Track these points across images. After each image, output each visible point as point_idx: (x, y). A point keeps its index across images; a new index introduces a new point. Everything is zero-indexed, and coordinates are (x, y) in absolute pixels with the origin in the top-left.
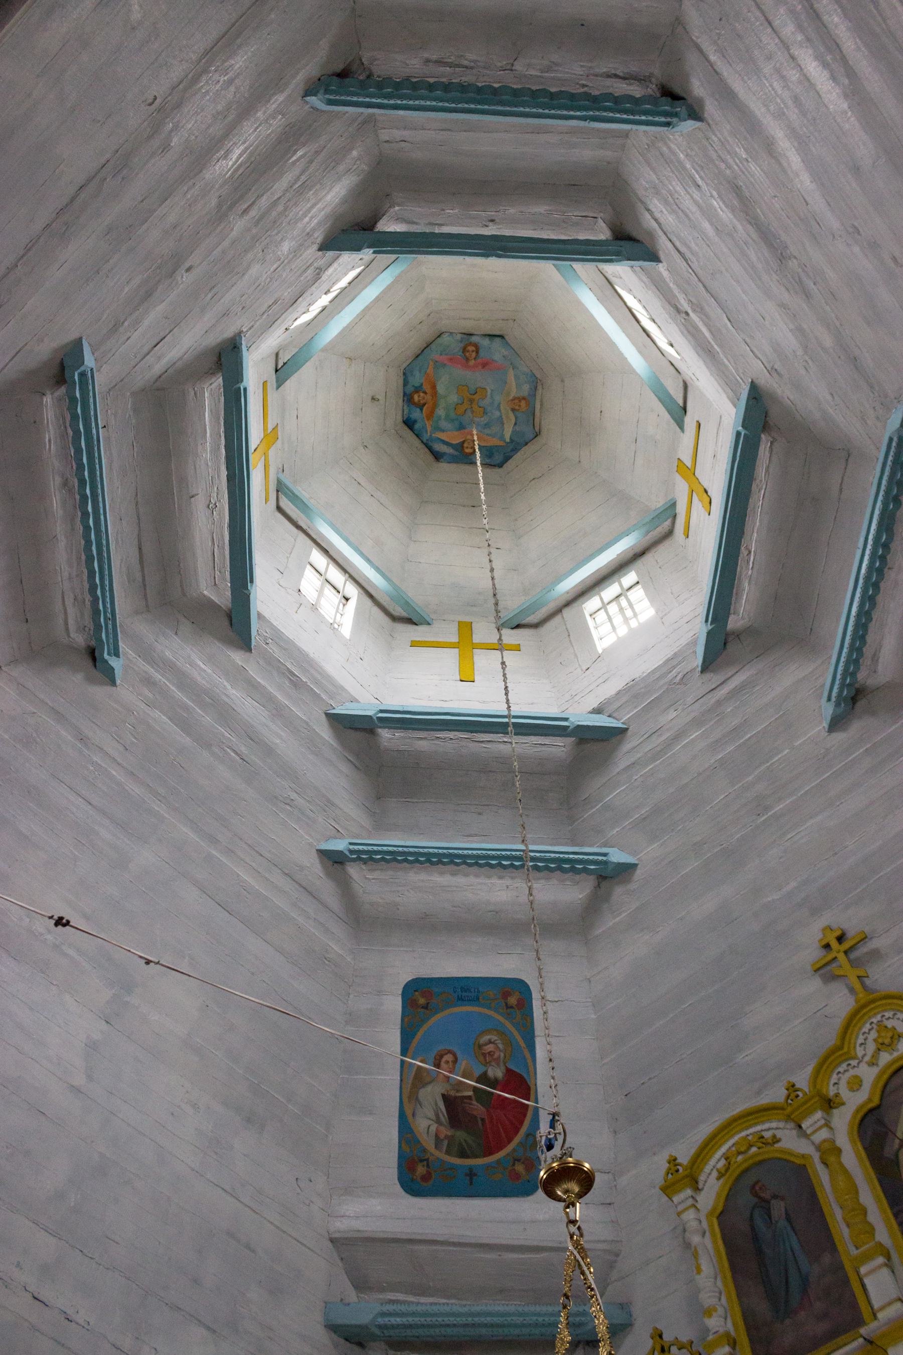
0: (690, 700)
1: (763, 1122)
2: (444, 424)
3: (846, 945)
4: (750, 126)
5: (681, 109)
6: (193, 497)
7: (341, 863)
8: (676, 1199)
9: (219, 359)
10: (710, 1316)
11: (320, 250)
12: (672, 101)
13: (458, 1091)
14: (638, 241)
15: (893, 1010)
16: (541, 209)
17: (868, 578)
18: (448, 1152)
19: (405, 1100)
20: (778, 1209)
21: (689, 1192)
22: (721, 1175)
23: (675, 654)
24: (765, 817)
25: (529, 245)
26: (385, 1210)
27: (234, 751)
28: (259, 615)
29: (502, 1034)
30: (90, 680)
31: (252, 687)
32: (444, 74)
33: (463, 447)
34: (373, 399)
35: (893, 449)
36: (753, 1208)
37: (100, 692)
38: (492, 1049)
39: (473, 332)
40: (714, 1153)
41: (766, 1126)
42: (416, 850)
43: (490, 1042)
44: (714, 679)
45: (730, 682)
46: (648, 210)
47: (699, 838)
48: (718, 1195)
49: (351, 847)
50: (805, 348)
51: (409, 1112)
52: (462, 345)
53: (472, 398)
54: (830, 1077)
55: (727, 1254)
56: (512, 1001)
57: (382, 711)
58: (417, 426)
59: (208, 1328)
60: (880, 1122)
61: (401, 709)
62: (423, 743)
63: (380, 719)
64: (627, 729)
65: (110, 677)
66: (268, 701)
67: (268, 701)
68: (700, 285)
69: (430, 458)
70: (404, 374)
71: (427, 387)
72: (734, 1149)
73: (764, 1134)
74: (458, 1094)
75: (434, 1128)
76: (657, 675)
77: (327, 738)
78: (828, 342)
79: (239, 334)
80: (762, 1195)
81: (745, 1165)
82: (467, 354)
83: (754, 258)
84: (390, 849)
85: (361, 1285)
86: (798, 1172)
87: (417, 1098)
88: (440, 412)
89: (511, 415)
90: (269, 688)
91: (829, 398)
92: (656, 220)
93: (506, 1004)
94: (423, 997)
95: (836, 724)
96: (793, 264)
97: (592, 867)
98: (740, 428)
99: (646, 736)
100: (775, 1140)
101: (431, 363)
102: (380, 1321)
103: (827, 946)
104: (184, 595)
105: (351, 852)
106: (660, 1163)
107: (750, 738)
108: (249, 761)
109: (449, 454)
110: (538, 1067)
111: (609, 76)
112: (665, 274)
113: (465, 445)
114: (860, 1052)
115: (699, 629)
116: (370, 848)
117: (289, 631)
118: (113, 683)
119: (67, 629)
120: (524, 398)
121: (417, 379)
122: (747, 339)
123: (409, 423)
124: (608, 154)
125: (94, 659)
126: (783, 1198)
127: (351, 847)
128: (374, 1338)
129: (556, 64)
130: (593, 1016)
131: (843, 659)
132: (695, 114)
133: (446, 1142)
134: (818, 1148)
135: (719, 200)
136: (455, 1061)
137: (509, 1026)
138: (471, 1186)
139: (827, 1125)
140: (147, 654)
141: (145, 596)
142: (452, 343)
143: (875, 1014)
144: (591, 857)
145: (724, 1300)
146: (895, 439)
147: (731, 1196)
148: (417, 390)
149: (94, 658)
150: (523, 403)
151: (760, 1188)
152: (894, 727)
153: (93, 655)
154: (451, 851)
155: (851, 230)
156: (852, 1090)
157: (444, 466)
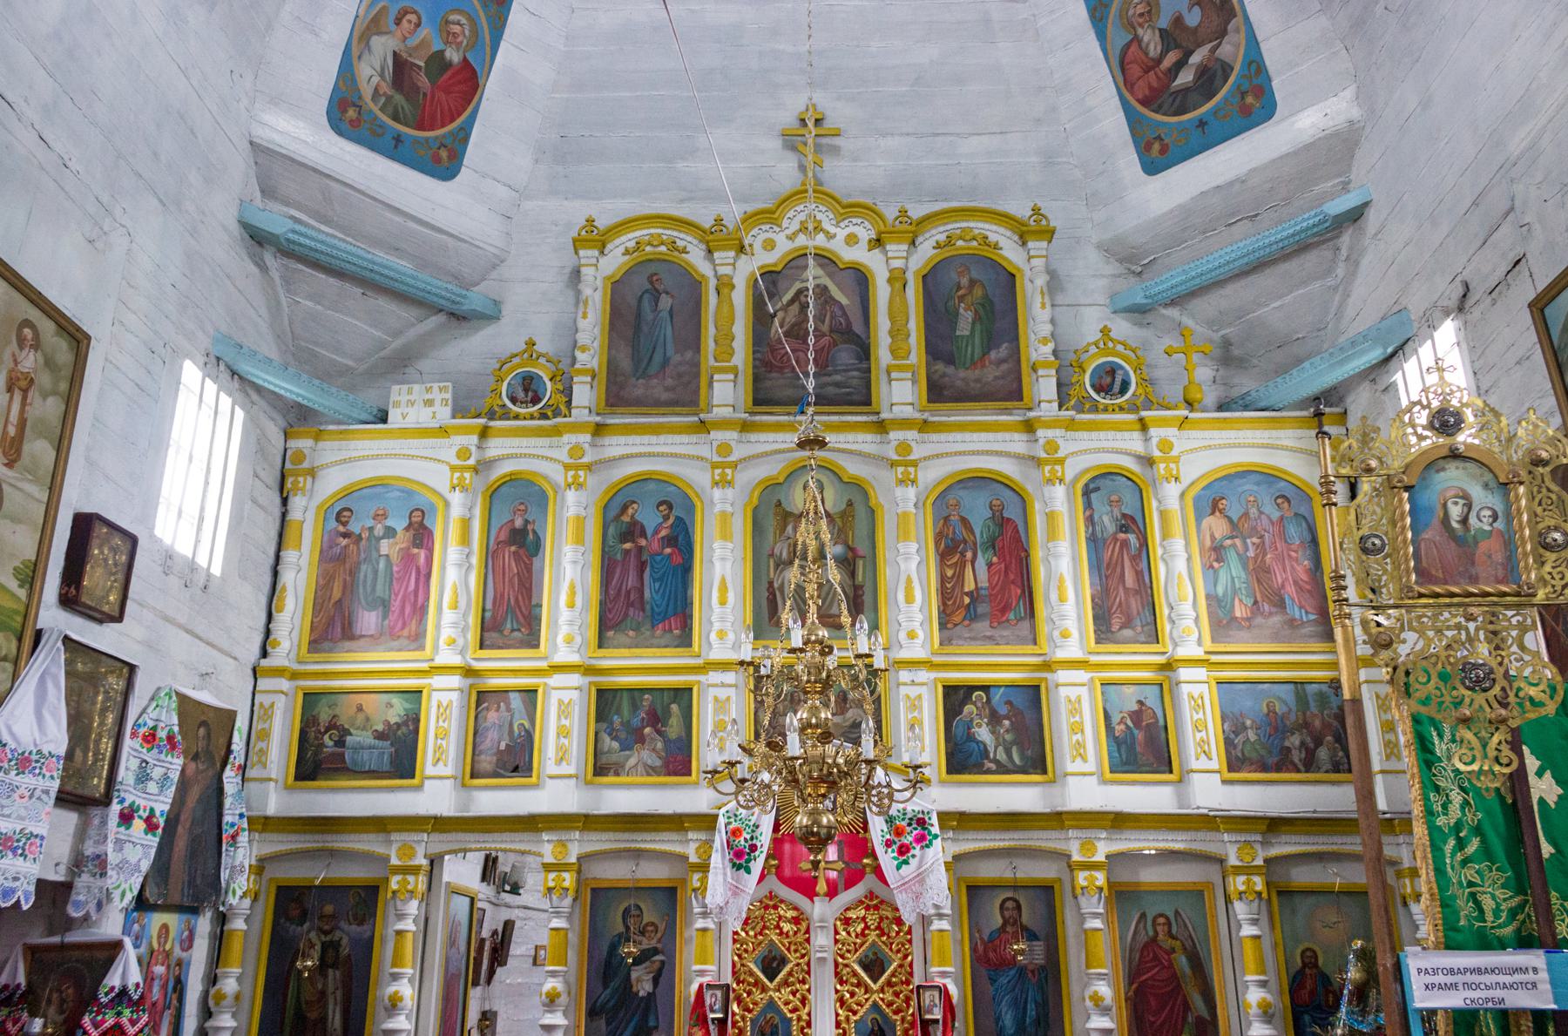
19: (355, 43)
20: (665, 302)
21: (596, 253)
22: (627, 252)
26: (305, 134)
29: (473, 21)
48: (620, 268)
51: (355, 52)
59: (161, 201)
75: (376, 79)
85: (268, 192)
86: (694, 286)
102: (291, 236)
106: (576, 212)
128: (270, 243)
133: (383, 100)
136: (418, 25)
137: (482, 14)
138: (395, 150)
156: (765, 248)
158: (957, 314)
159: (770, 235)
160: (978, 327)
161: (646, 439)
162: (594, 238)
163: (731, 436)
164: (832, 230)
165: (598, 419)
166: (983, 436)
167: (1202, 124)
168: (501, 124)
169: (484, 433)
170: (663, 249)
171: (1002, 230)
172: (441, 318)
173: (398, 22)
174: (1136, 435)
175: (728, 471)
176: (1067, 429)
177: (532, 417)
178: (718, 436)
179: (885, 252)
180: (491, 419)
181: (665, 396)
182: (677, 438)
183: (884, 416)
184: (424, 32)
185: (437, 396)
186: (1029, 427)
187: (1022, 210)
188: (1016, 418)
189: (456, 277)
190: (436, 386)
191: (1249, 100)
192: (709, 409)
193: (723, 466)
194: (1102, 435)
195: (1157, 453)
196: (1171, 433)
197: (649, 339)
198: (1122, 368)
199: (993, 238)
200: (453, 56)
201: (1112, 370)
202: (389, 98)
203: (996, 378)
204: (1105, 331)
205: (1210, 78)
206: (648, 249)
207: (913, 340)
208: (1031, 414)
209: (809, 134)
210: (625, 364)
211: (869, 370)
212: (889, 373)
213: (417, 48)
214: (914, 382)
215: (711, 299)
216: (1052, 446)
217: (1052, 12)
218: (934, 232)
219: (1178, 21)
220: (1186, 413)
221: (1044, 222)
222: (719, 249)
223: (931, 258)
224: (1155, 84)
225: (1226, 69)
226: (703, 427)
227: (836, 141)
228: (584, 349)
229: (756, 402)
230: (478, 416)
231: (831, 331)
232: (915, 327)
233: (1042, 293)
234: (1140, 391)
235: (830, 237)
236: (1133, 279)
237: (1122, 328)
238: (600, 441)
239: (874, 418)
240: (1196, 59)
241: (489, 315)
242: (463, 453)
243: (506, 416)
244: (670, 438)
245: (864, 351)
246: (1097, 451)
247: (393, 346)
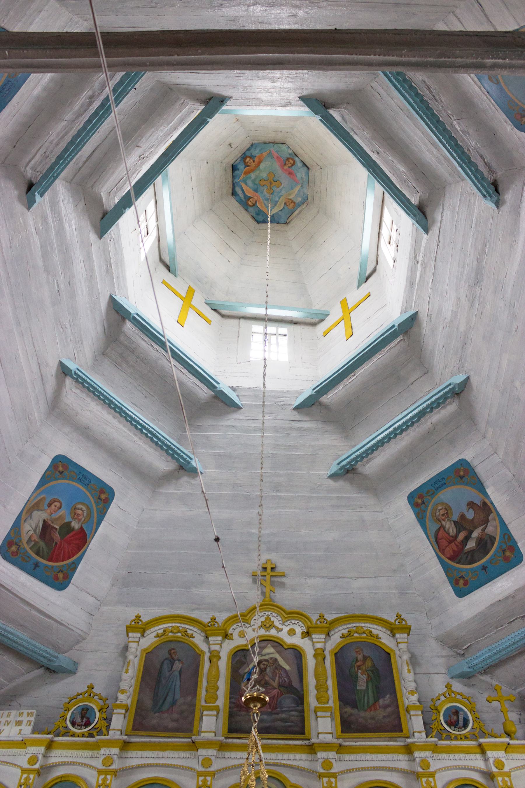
0: (279, 417)
1: (190, 625)
2: (249, 182)
3: (273, 574)
4: (514, 230)
5: (495, 198)
6: (138, 146)
7: (66, 375)
9: (210, 99)
10: (123, 693)
11: (299, 97)
12: (494, 190)
13: (52, 523)
14: (425, 217)
15: (278, 614)
16: (402, 168)
17: (396, 429)
18: (31, 548)
20: (177, 666)
21: (139, 635)
22: (157, 636)
23: (288, 391)
24: (275, 494)
25: (387, 181)
27: (57, 283)
28: (118, 223)
29: (89, 509)
31: (89, 257)
32: (424, 91)
33: (249, 200)
34: (230, 145)
35: (448, 389)
36: (166, 659)
37: (19, 208)
38: (80, 513)
39: (299, 156)
40: (160, 625)
41: (191, 628)
42: (107, 395)
43: (81, 509)
44: (296, 416)
45: (303, 423)
46: (443, 212)
47: (239, 482)
49: (77, 371)
50: (451, 321)
51: (23, 517)
52: (289, 156)
53: (272, 182)
54: (233, 625)
55: (143, 671)
56: (103, 496)
58: (237, 172)
60: (245, 657)
61: (147, 320)
62: (144, 344)
63: (134, 317)
64: (242, 408)
65: (30, 204)
66: (90, 270)
67: (90, 270)
68: (434, 258)
69: (231, 191)
70: (252, 145)
71: (256, 160)
72: (170, 628)
73: (188, 631)
74: (52, 524)
75: (31, 533)
76: (273, 394)
77: (102, 308)
78: (462, 328)
79: (230, 98)
80: (173, 656)
81: (171, 639)
82: (287, 162)
83: (466, 272)
84: (95, 386)
86: (196, 657)
87: (31, 514)
88: (253, 175)
89: (283, 205)
90: (95, 264)
91: (441, 347)
92: (442, 219)
93: (99, 496)
94: (62, 467)
95: (334, 476)
96: (478, 290)
97: (181, 460)
98: (396, 325)
99: (247, 418)
100: (192, 636)
101: (268, 151)
103: (265, 569)
104: (92, 186)
105: (75, 373)
107: (293, 454)
108: (61, 294)
109: (240, 198)
110: (96, 534)
111: (482, 157)
112: (424, 241)
113: (251, 200)
114: (252, 623)
115: (308, 392)
116: (86, 378)
117: (124, 242)
118: (29, 208)
119: (28, 164)
120: (294, 203)
121: (255, 152)
122: (432, 295)
123: (234, 168)
124: (449, 178)
126: (182, 663)
127: (77, 371)
129: (468, 133)
130: (135, 527)
131: (358, 453)
132: (498, 204)
133: (33, 543)
134: (210, 651)
135: (474, 240)
136: (60, 508)
138: (34, 571)
139: (221, 645)
140: (54, 205)
141: (76, 174)
142: (285, 152)
143: (269, 611)
144: (184, 456)
145: (131, 690)
146: (452, 386)
147: (158, 647)
148: (251, 157)
149: (30, 189)
150: (292, 205)
151: (174, 653)
152: (355, 495)
153: (30, 186)
154: (123, 408)
155: (512, 303)
158: (357, 677)
160: (370, 684)
161: (155, 754)
162: (139, 627)
163: (211, 752)
164: (280, 626)
165: (125, 737)
166: (380, 756)
167: (484, 568)
168: (95, 566)
169: (50, 746)
170: (179, 634)
171: (380, 628)
172: (41, 671)
173: (49, 505)
174: (478, 756)
175: (209, 778)
176: (434, 751)
177: (83, 736)
178: (203, 752)
179: (312, 639)
180: (58, 735)
181: (172, 725)
182: (176, 754)
183: (314, 740)
184: (62, 512)
185: (25, 718)
186: (409, 750)
187: (392, 618)
188: (400, 743)
189: (55, 647)
190: (26, 712)
192: (200, 732)
193: (204, 774)
194: (457, 756)
195: (494, 769)
196: (500, 754)
197: (165, 692)
199: (375, 632)
200: (76, 525)
202: (36, 543)
203: (384, 717)
204: (448, 686)
205: (485, 545)
206: (170, 634)
207: (330, 692)
208: (409, 740)
209: (269, 575)
210: (148, 702)
211: (303, 711)
212: (316, 712)
213: (57, 519)
214: (332, 719)
215: (206, 665)
216: (425, 764)
217: (397, 516)
218: (340, 628)
220: (507, 740)
221: (404, 623)
223: (339, 644)
224: (456, 549)
225: (492, 539)
226: (194, 746)
227: (283, 580)
228: (123, 692)
229: (230, 731)
230: (49, 733)
231: (280, 686)
232: (331, 683)
233: (407, 663)
234: (476, 725)
235: (279, 630)
236: (459, 659)
237: (457, 686)
238: (125, 754)
239: (307, 742)
241: (68, 672)
242: (33, 760)
243: (67, 733)
244: (171, 754)
245: (300, 699)
246: (456, 768)
247: (7, 688)
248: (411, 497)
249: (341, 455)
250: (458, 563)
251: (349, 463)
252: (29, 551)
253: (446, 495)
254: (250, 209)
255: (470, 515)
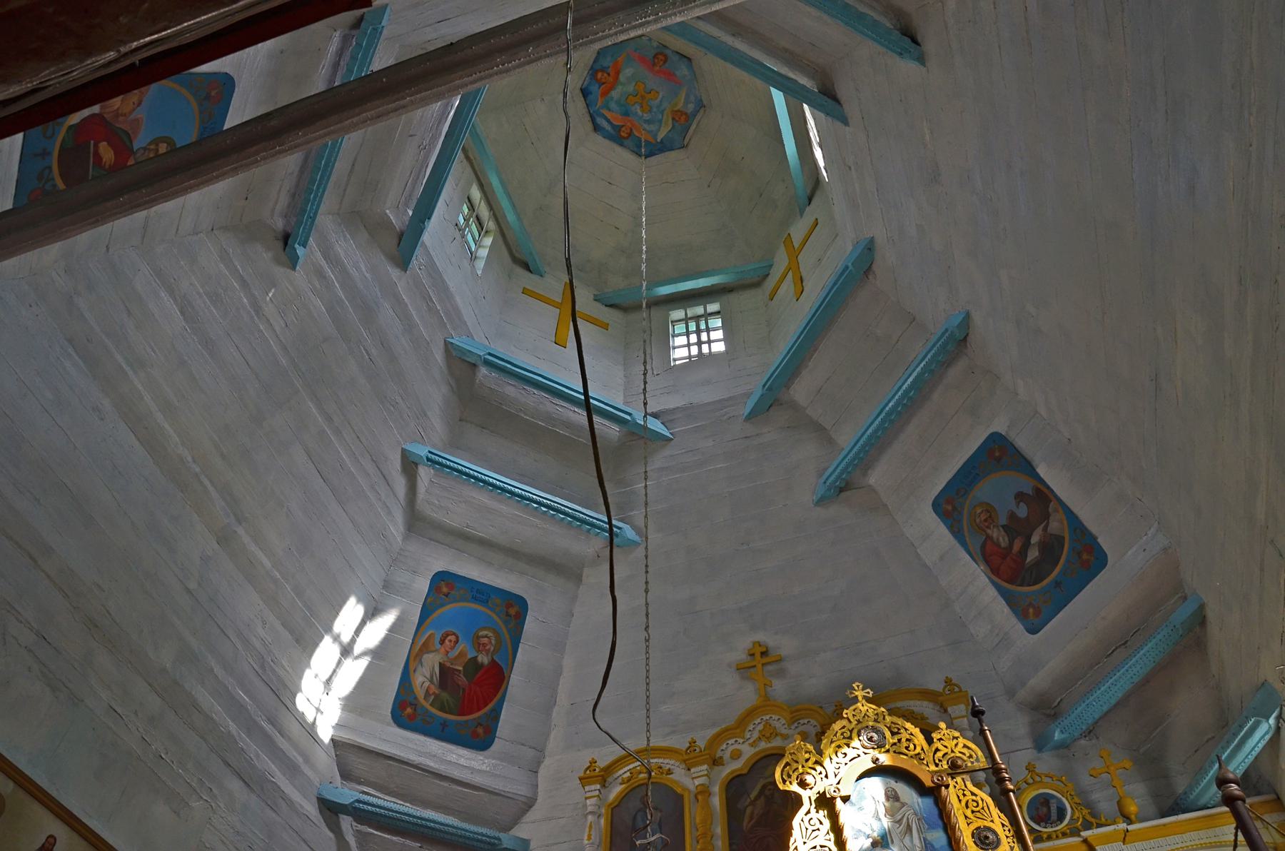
2: (613, 105)
3: (765, 660)
8: (587, 788)
21: (598, 786)
30: (278, 262)
37: (280, 272)
51: (411, 668)
56: (512, 611)
57: (490, 354)
58: (591, 97)
65: (293, 262)
75: (427, 684)
85: (346, 775)
86: (676, 800)
88: (615, 94)
89: (670, 121)
95: (821, 502)
106: (584, 758)
118: (294, 268)
121: (607, 62)
125: (286, 244)
132: (921, 60)
136: (457, 642)
140: (328, 253)
148: (603, 70)
153: (286, 239)
157: (599, 138)
159: (736, 746)
162: (603, 776)
164: (785, 732)
167: (1057, 584)
173: (442, 642)
184: (461, 647)
187: (936, 684)
191: (1085, 556)
198: (1053, 796)
200: (484, 659)
201: (1044, 800)
202: (437, 696)
205: (1051, 548)
219: (1012, 516)
220: (1123, 826)
222: (696, 765)
225: (1060, 540)
240: (1035, 539)
248: (936, 506)
249: (825, 469)
250: (1021, 585)
251: (839, 477)
252: (430, 708)
253: (985, 491)
254: (626, 142)
255: (1022, 511)
